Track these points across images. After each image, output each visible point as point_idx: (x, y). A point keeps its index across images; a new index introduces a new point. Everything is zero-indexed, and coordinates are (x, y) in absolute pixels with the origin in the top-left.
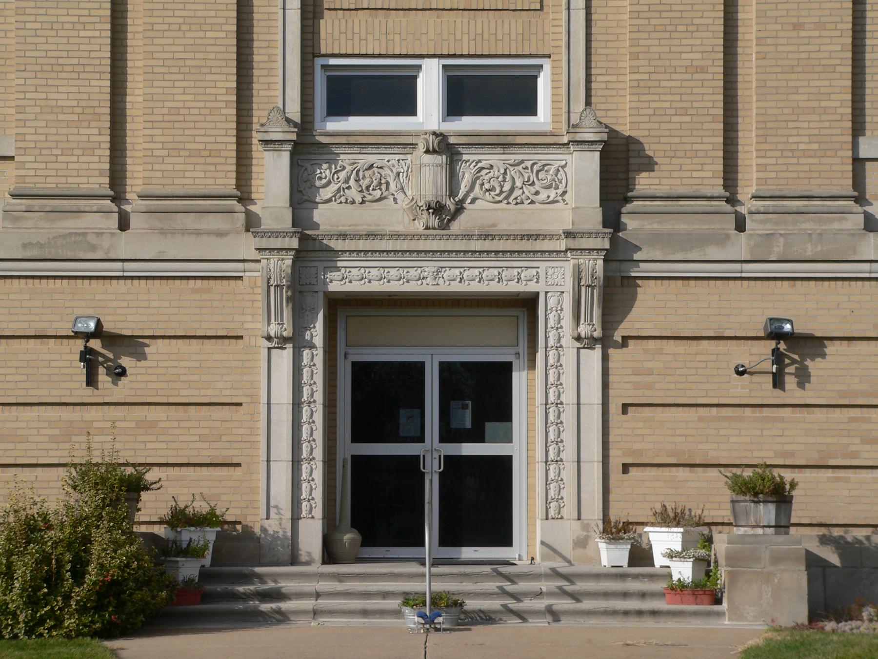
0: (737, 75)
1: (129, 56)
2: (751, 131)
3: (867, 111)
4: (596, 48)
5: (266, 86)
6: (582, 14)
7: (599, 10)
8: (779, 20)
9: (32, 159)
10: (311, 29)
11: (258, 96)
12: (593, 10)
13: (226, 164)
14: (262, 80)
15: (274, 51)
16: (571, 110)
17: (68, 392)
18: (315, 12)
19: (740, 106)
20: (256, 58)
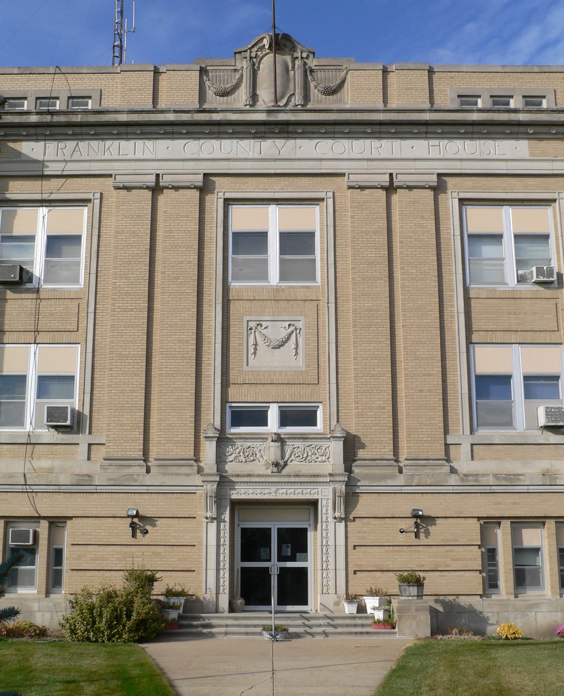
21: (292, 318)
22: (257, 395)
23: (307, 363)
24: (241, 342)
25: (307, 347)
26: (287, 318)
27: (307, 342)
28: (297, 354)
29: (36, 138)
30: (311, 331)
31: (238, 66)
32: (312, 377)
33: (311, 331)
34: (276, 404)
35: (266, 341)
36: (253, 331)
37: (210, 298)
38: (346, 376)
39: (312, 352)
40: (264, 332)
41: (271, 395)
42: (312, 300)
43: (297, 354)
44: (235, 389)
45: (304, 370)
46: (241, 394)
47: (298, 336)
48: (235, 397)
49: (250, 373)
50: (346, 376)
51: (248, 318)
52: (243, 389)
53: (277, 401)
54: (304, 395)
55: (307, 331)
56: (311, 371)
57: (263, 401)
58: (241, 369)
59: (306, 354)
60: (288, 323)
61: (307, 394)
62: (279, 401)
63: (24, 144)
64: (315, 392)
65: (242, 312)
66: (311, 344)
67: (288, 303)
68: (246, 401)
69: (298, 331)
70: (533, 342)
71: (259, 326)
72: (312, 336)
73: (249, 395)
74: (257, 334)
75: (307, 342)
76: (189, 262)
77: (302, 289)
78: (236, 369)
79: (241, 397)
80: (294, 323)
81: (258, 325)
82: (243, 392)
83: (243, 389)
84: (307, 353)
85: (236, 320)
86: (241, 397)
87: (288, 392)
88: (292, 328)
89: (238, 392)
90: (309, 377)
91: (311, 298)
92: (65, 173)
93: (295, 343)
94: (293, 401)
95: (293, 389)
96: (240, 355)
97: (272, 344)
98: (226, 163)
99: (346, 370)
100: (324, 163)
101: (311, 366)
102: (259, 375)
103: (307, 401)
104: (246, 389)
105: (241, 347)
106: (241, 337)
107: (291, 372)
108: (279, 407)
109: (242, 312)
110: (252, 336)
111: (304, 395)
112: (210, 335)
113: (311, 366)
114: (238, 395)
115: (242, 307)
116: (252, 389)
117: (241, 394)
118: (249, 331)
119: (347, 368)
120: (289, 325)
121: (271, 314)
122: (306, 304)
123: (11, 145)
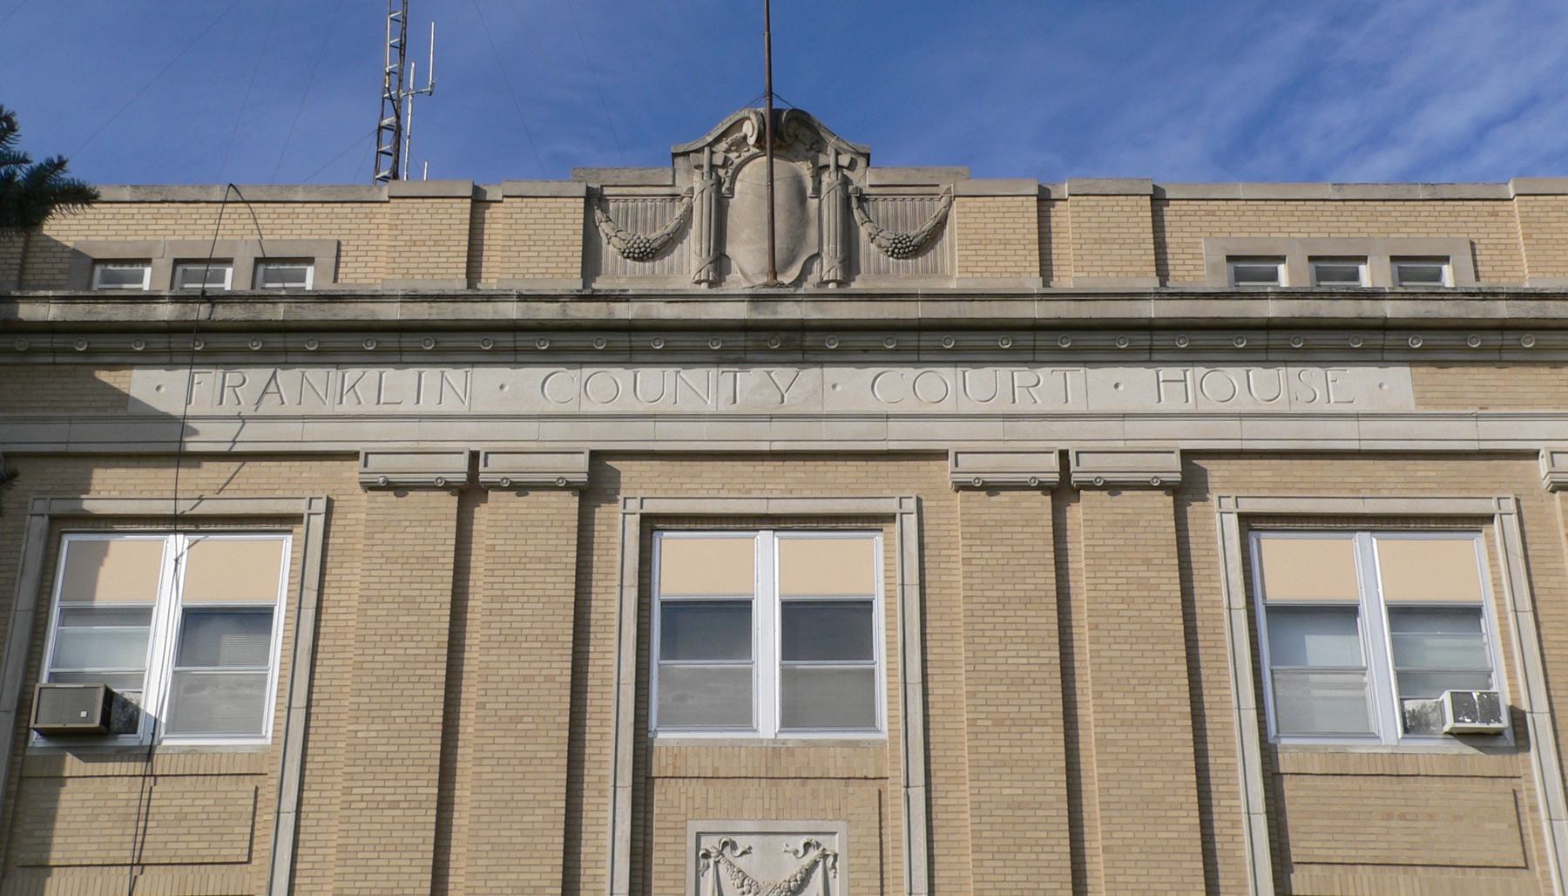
0: (1083, 826)
1: (468, 629)
2: (1096, 820)
3: (1217, 852)
4: (936, 784)
5: (597, 765)
6: (916, 590)
7: (941, 816)
8: (1085, 269)
9: (364, 727)
10: (643, 752)
11: (589, 760)
12: (934, 816)
13: (554, 829)
14: (593, 744)
15: (607, 730)
16: (908, 681)
17: (454, 205)
18: (645, 849)
19: (1086, 830)
20: (583, 850)
29: (169, 359)
31: (681, 188)
36: (711, 861)
40: (741, 863)
42: (866, 778)
47: (831, 874)
55: (852, 861)
60: (805, 839)
63: (137, 374)
67: (803, 785)
71: (728, 848)
72: (866, 875)
74: (722, 867)
76: (549, 679)
81: (725, 844)
88: (814, 854)
92: (238, 448)
98: (649, 425)
100: (892, 424)
106: (681, 876)
115: (683, 797)
118: (702, 861)
120: (807, 845)
123: (104, 376)
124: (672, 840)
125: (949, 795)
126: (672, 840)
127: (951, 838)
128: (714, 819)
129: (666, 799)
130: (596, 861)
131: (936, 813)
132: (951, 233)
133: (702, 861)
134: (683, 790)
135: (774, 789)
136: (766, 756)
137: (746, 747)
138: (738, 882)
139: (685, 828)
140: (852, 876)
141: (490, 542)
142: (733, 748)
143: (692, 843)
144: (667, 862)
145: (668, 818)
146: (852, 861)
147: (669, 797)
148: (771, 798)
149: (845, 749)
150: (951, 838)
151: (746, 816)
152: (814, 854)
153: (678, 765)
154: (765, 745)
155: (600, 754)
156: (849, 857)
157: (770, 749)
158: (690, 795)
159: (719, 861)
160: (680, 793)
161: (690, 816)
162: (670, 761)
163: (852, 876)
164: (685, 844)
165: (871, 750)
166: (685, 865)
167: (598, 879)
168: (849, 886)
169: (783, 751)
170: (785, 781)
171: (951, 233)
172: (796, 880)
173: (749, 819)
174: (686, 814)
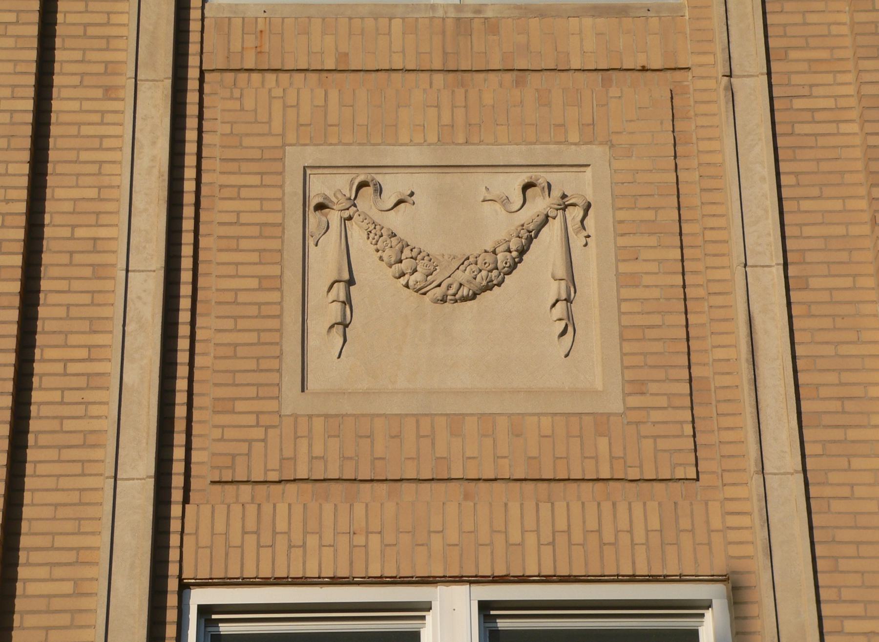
21: (540, 153)
22: (360, 540)
23: (630, 375)
24: (275, 270)
25: (625, 293)
26: (516, 154)
27: (624, 268)
28: (569, 327)
30: (649, 215)
32: (662, 444)
33: (649, 215)
34: (464, 589)
35: (405, 266)
36: (334, 217)
37: (109, 56)
38: (852, 434)
39: (656, 320)
40: (396, 221)
41: (436, 542)
42: (644, 69)
43: (569, 327)
44: (236, 509)
45: (617, 406)
46: (266, 539)
47: (577, 242)
48: (235, 555)
49: (318, 425)
50: (852, 434)
51: (312, 155)
52: (282, 508)
53: (469, 571)
54: (625, 539)
55: (621, 215)
56: (656, 416)
57: (390, 571)
58: (272, 405)
59: (623, 328)
60: (524, 177)
61: (640, 535)
62: (485, 571)
64: (685, 523)
65: (277, 127)
66: (647, 280)
67: (518, 83)
68: (296, 572)
69: (575, 214)
70: (406, 571)
71: (368, 191)
72: (653, 241)
73: (312, 541)
74: (356, 233)
75: (624, 268)
77: (588, 22)
78: (240, 406)
79: (266, 554)
80: (553, 177)
81: (363, 185)
82: (282, 526)
83: (282, 508)
84: (626, 321)
85: (245, 167)
86: (266, 554)
87: (530, 523)
88: (539, 204)
89: (251, 525)
90: (648, 444)
91: (641, 61)
93: (561, 272)
94: (563, 571)
95: (560, 507)
96: (266, 337)
97: (437, 277)
99: (850, 406)
101: (645, 254)
102: (370, 436)
103: (642, 570)
104: (298, 510)
105: (274, 296)
106: (274, 244)
107: (546, 422)
108: (485, 607)
109: (277, 127)
110: (332, 241)
111: (625, 539)
112: (103, 232)
113: (653, 388)
114: (297, 539)
115: (277, 105)
116: (328, 508)
117: (266, 539)
118: (314, 218)
119: (858, 391)
121: (433, 138)
122: (614, 91)
124: (255, 180)
125: (816, 91)
126: (255, 180)
127: (825, 166)
128: (340, 143)
129: (242, 109)
130: (98, 214)
131: (23, 613)
132: (349, 229)
133: (314, 218)
134: (278, 92)
135: (460, 92)
136: (444, 33)
137: (403, 19)
138: (389, 254)
139: (282, 160)
140: (622, 241)
141: (221, 392)
142: (376, 19)
143: (293, 185)
144: (244, 218)
145: (247, 141)
146: (621, 215)
147: (249, 104)
148: (453, 107)
149: (598, 20)
150: (825, 166)
151: (404, 138)
152: (539, 204)
153: (266, 48)
154: (440, 13)
155: (108, 24)
156: (615, 209)
157: (450, 23)
158: (291, 100)
159: (350, 218)
160: (271, 98)
161: (291, 137)
162: (251, 41)
163: (622, 241)
164: (281, 187)
165: (654, 22)
166: (281, 225)
167: (100, 245)
168: (617, 261)
169: (476, 24)
170: (482, 76)
171: (349, 229)
172: (509, 251)
173: (411, 143)
174: (283, 135)
